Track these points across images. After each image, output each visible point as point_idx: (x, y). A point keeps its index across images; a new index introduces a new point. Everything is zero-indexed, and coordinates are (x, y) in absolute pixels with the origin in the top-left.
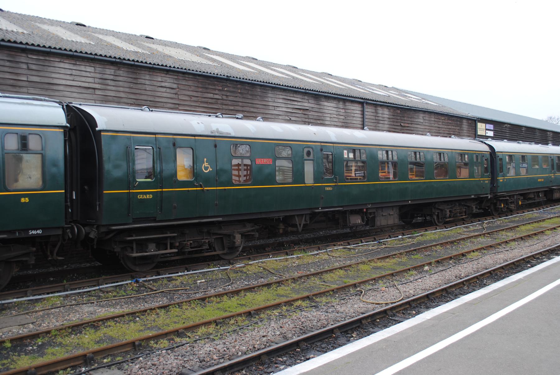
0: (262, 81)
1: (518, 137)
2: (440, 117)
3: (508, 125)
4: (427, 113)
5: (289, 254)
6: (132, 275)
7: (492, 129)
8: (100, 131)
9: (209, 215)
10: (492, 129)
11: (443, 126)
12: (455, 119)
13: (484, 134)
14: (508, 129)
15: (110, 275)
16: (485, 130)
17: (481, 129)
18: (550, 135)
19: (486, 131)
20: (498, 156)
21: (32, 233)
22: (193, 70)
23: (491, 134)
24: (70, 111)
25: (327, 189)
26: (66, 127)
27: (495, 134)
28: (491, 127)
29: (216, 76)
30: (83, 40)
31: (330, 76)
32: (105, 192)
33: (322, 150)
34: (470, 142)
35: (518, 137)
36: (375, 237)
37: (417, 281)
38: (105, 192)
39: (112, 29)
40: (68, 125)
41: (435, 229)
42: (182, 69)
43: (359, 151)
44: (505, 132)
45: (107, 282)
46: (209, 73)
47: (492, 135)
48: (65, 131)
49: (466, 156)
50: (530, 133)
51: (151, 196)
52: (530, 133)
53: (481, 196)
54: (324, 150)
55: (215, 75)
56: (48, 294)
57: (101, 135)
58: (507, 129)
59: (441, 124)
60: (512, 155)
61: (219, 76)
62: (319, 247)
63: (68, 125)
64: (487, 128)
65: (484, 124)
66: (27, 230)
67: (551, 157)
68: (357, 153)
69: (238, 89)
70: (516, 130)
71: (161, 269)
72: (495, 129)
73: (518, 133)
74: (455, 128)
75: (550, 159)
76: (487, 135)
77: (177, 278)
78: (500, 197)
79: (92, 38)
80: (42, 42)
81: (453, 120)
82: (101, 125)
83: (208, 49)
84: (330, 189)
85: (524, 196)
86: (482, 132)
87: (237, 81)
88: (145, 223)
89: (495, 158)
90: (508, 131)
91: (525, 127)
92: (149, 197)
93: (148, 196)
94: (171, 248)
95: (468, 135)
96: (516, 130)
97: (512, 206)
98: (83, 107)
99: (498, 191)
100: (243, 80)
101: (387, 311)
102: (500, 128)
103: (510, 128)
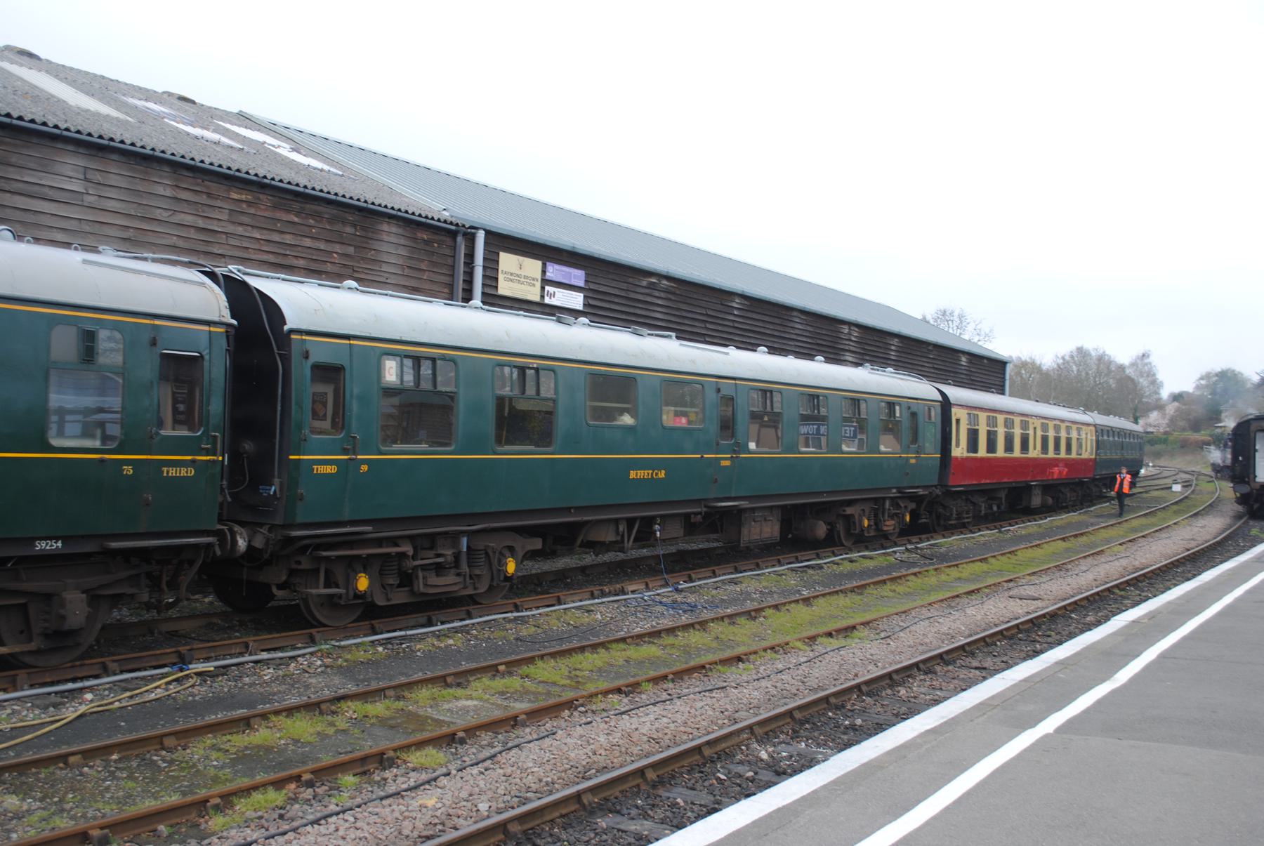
0: (417, 214)
1: (708, 326)
2: (214, 187)
3: (665, 282)
4: (115, 157)
5: (520, 609)
6: (515, 603)
7: (581, 283)
8: (292, 331)
9: (733, 495)
10: (581, 283)
11: (231, 228)
12: (327, 211)
13: (537, 298)
14: (662, 295)
15: (278, 633)
16: (538, 284)
17: (513, 277)
18: (849, 334)
19: (547, 288)
20: (306, 356)
21: (58, 547)
22: (351, 198)
23: (576, 300)
24: (238, 293)
25: (322, 469)
26: (229, 325)
27: (592, 302)
28: (577, 276)
29: (302, 190)
30: (104, 109)
31: (26, 59)
32: (291, 457)
33: (154, 343)
34: (85, 261)
35: (708, 326)
36: (759, 561)
37: (299, 831)
38: (291, 457)
39: (99, 73)
40: (235, 322)
41: (423, 620)
42: (380, 205)
43: (429, 363)
44: (722, 319)
45: (444, 619)
46: (128, 142)
47: (580, 307)
48: (227, 332)
49: (897, 408)
50: (767, 319)
51: (191, 472)
52: (767, 319)
53: (115, 545)
54: (159, 343)
55: (148, 151)
56: (538, 608)
57: (290, 339)
58: (656, 293)
59: (225, 217)
60: (859, 400)
61: (158, 154)
62: (558, 597)
63: (235, 322)
64: (550, 275)
65: (539, 264)
66: (34, 539)
67: (909, 408)
68: (426, 370)
69: (198, 185)
70: (703, 304)
71: (378, 621)
72: (592, 286)
73: (710, 313)
74: (329, 247)
75: (711, 395)
76: (547, 300)
77: (824, 565)
78: (319, 547)
79: (120, 106)
80: (180, 150)
81: (317, 216)
82: (293, 320)
83: (31, 55)
84: (329, 471)
85: (1048, 488)
86: (526, 288)
87: (419, 224)
88: (162, 539)
89: (286, 360)
90: (660, 302)
91: (744, 297)
92: (187, 472)
93: (184, 470)
94: (327, 586)
95: (413, 283)
96: (703, 304)
97: (889, 525)
98: (254, 282)
99: (300, 519)
100: (343, 200)
101: (646, 771)
102: (624, 286)
103: (673, 293)
